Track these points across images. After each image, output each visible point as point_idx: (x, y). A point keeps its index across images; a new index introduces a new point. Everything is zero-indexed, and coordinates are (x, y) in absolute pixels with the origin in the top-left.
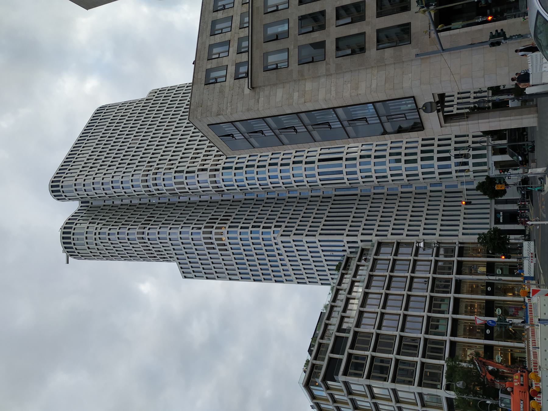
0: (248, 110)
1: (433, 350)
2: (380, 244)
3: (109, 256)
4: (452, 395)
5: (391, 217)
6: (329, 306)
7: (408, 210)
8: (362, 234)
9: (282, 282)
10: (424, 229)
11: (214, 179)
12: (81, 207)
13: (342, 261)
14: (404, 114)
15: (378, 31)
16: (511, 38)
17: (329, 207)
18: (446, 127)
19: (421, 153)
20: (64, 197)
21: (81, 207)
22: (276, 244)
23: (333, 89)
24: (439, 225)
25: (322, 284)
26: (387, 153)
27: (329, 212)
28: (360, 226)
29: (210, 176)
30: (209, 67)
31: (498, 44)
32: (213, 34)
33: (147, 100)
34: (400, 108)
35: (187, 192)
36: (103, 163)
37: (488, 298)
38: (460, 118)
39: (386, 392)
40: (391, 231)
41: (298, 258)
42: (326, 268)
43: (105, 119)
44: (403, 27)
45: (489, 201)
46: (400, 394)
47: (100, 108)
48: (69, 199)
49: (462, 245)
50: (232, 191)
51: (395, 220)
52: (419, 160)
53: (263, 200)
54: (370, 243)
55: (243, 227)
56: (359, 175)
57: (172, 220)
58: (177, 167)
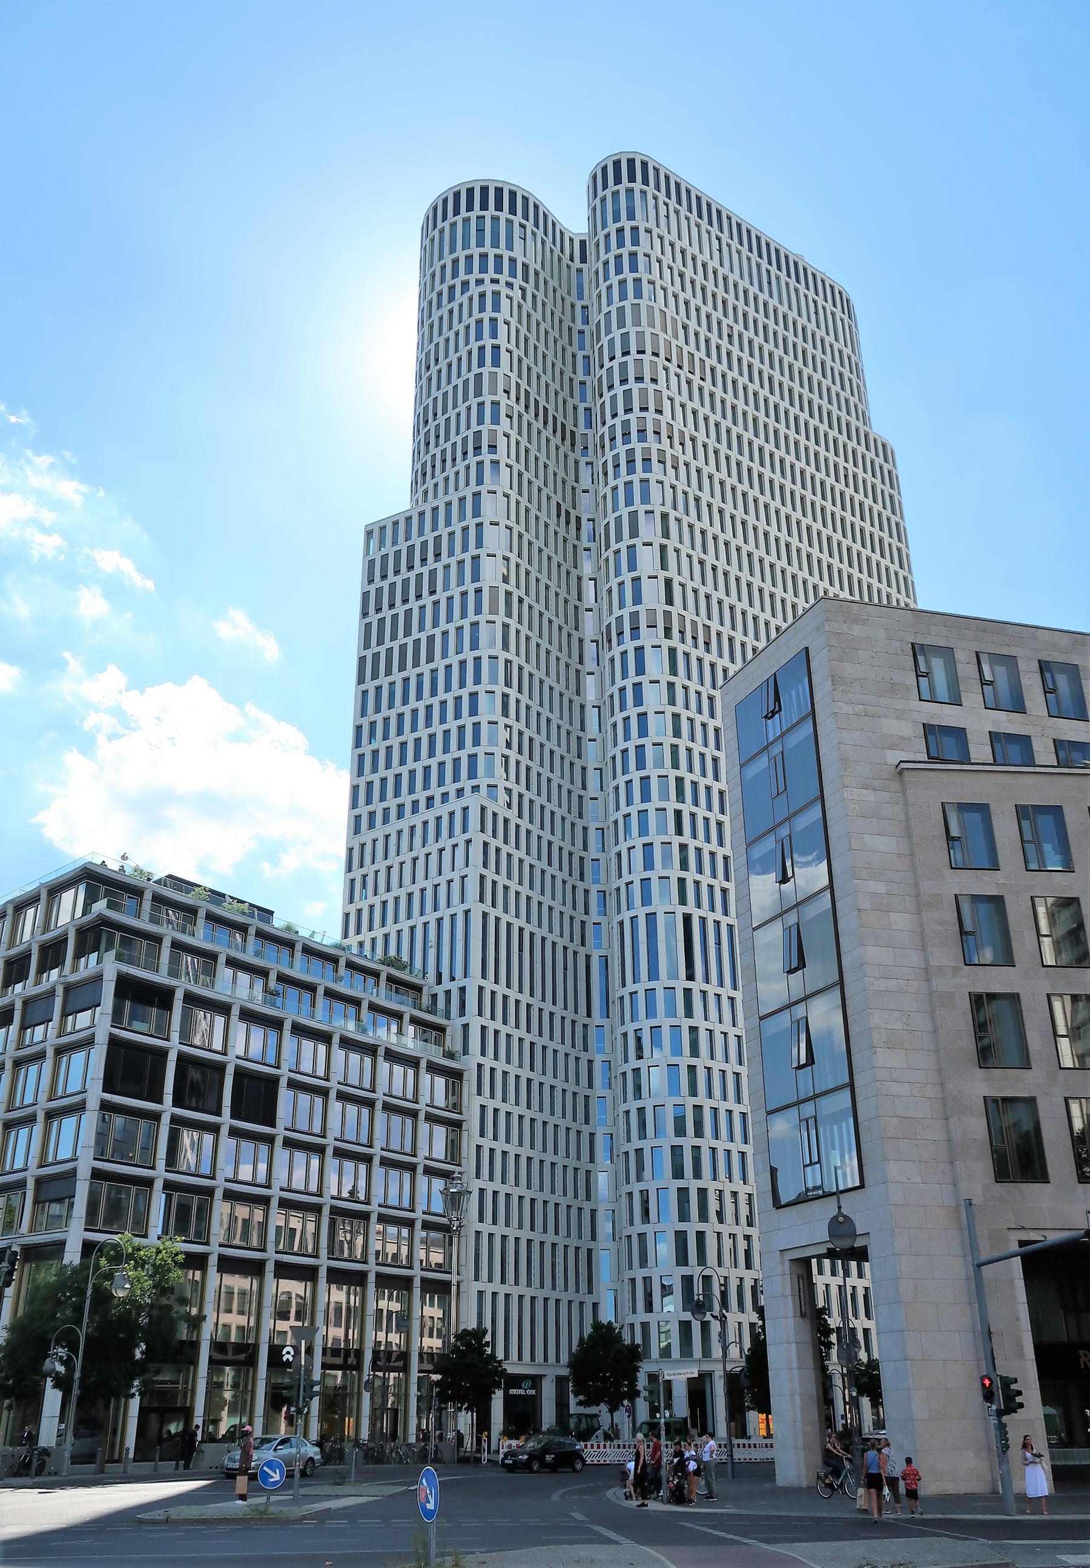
0: (844, 760)
1: (183, 1212)
2: (455, 1076)
3: (430, 317)
4: (72, 1256)
5: (529, 1107)
6: (294, 937)
7: (545, 1150)
8: (484, 1028)
9: (354, 804)
10: (495, 1193)
11: (643, 623)
12: (571, 240)
13: (411, 973)
14: (819, 1162)
15: (1031, 1101)
16: (1002, 1428)
17: (558, 940)
18: (782, 1263)
20: (600, 194)
21: (571, 240)
22: (460, 792)
23: (891, 984)
24: (506, 1231)
25: (347, 916)
27: (543, 939)
28: (505, 1022)
29: (652, 612)
30: (959, 655)
31: (988, 1396)
32: (1044, 667)
33: (866, 436)
34: (833, 1148)
35: (608, 547)
36: (667, 243)
37: (365, 1356)
38: (802, 1297)
39: (74, 1086)
40: (491, 1105)
41: (419, 852)
42: (391, 928)
43: (816, 313)
44: (1033, 1141)
45: (565, 1358)
46: (69, 1123)
47: (847, 301)
48: (594, 209)
49: (454, 1289)
50: (608, 671)
51: (521, 1117)
52: (681, 1183)
53: (579, 757)
54: (458, 1047)
55: (507, 701)
57: (530, 501)
58: (678, 520)
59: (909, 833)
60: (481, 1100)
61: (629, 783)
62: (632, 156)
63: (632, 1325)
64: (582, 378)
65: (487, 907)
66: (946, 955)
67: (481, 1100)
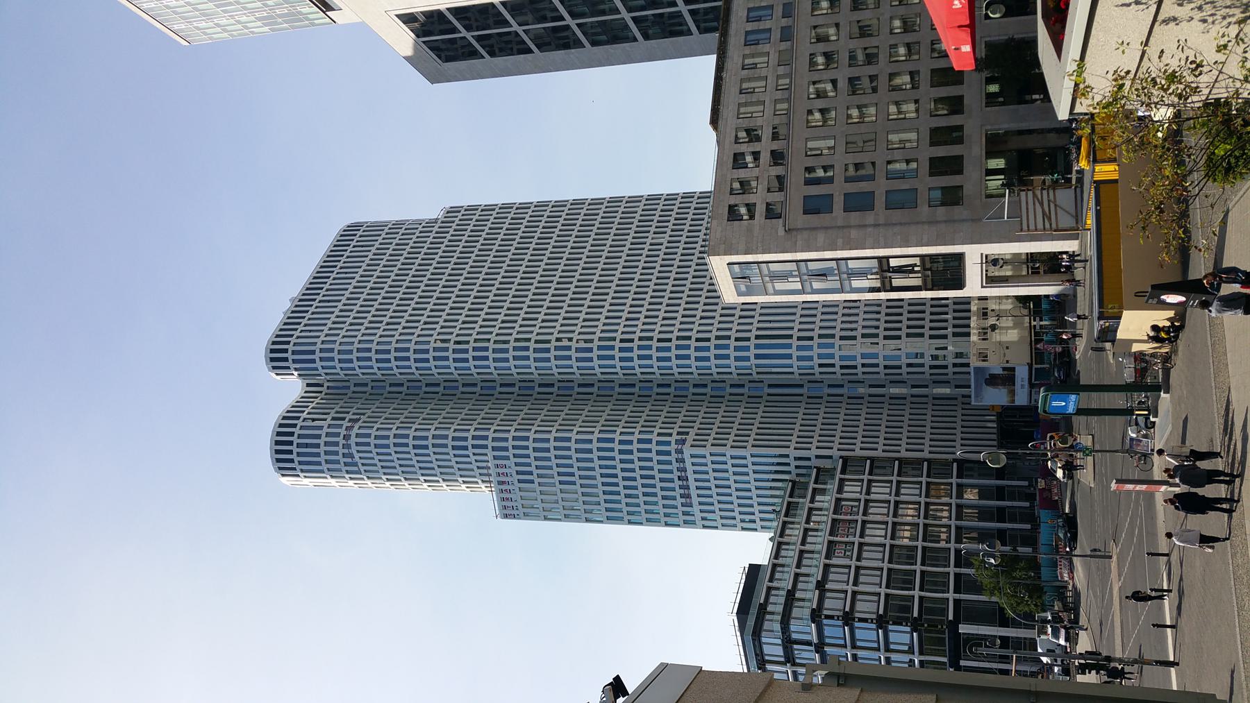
12: (306, 392)
19: (856, 337)
21: (306, 392)
26: (815, 334)
47: (349, 227)
56: (596, 363)
60: (813, 448)
61: (600, 366)
62: (269, 351)
64: (479, 388)
65: (709, 444)
66: (869, 218)
67: (857, 450)
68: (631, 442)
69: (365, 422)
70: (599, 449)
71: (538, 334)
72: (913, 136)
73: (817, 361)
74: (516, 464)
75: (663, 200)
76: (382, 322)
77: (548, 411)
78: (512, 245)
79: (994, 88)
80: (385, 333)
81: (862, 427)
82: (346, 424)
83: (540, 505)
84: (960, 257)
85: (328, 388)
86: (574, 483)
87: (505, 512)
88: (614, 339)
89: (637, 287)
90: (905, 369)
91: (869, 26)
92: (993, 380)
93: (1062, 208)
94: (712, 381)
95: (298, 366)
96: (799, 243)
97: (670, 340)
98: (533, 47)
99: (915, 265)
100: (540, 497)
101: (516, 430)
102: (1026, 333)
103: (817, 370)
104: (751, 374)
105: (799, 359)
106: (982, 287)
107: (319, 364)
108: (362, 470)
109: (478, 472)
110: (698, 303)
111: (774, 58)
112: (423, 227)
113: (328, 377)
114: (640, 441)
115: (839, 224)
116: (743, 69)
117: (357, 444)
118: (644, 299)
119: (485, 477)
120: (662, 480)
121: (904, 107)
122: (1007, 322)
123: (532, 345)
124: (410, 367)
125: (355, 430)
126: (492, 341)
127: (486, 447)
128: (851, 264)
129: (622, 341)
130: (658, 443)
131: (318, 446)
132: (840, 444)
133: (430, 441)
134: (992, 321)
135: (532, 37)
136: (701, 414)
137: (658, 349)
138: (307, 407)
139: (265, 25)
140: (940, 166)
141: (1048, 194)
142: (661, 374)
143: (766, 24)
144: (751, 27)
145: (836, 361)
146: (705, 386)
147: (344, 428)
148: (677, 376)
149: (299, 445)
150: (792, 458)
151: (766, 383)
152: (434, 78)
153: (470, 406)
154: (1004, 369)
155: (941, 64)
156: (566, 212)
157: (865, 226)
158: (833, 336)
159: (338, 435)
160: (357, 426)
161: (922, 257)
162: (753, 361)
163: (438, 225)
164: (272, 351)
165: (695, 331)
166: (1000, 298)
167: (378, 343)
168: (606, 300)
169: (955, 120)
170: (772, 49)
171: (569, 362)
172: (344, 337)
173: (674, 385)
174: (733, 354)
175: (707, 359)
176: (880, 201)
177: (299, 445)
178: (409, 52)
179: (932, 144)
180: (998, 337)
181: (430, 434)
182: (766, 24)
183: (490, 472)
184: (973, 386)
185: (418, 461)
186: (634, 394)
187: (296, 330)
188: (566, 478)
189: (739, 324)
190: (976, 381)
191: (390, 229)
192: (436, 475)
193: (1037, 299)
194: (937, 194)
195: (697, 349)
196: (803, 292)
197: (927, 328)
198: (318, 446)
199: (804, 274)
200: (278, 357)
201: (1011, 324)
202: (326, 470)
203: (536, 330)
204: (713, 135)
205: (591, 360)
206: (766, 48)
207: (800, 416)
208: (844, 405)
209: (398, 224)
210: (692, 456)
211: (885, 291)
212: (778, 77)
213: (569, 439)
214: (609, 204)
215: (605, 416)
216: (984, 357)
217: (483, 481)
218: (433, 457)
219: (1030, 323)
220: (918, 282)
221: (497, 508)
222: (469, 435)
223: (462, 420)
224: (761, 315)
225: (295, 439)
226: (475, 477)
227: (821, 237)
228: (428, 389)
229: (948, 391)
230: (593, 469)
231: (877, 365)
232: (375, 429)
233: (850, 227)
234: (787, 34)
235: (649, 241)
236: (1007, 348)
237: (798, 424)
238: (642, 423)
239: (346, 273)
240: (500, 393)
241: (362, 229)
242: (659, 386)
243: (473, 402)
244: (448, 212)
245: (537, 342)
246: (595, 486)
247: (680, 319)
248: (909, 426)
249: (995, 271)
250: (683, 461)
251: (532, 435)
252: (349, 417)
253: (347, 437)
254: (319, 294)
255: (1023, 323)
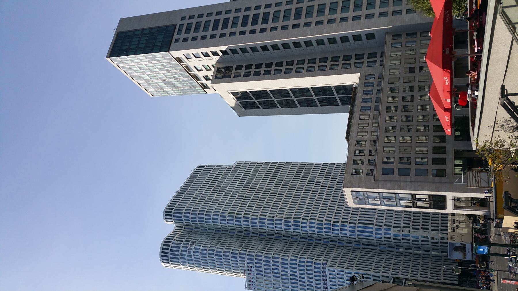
12: (176, 229)
19: (419, 228)
21: (176, 229)
59: (387, 181)
60: (381, 272)
63: (431, 246)
64: (229, 232)
66: (408, 178)
68: (304, 262)
69: (197, 243)
70: (290, 264)
71: (253, 212)
72: (425, 149)
73: (383, 236)
74: (256, 267)
75: (322, 165)
76: (209, 204)
77: (254, 244)
78: (261, 178)
79: (458, 134)
80: (210, 208)
81: (384, 263)
82: (190, 243)
83: (264, 285)
84: (444, 197)
85: (185, 228)
86: (279, 277)
87: (250, 287)
88: (266, 216)
89: (310, 198)
90: (420, 243)
91: (408, 106)
92: (457, 249)
93: (483, 180)
94: (339, 240)
95: (175, 218)
96: (380, 185)
97: (322, 221)
98: (279, 106)
99: (426, 198)
100: (282, 284)
101: (257, 252)
102: (471, 231)
103: (384, 239)
104: (356, 238)
105: (376, 234)
106: (453, 209)
107: (183, 218)
108: (194, 263)
109: (240, 268)
110: (305, 205)
111: (371, 117)
112: (228, 168)
113: (186, 224)
114: (308, 262)
115: (396, 180)
116: (359, 119)
117: (194, 252)
118: (313, 203)
119: (243, 271)
120: (316, 280)
121: (406, 138)
122: (463, 225)
123: (250, 216)
124: (218, 222)
125: (194, 246)
126: (235, 214)
127: (244, 258)
128: (401, 196)
129: (303, 219)
130: (315, 263)
131: (178, 251)
132: (347, 266)
133: (223, 253)
134: (457, 224)
135: (242, 104)
136: (318, 251)
137: (317, 224)
138: (176, 235)
139: (182, 92)
140: (436, 161)
141: (478, 174)
142: (318, 235)
143: (369, 104)
144: (363, 105)
145: (391, 236)
146: (336, 242)
147: (189, 245)
148: (324, 236)
149: (171, 250)
150: (372, 275)
151: (387, 245)
152: (240, 114)
153: (224, 239)
154: (462, 244)
155: (437, 123)
156: (283, 167)
157: (407, 181)
158: (390, 226)
159: (186, 247)
160: (194, 244)
161: (429, 195)
162: (357, 233)
163: (233, 168)
164: (166, 212)
165: (333, 218)
166: (460, 215)
167: (221, 213)
168: (297, 202)
169: (443, 145)
170: (371, 113)
171: (298, 228)
172: (194, 208)
173: (338, 241)
174: (316, 226)
175: (337, 230)
176: (413, 172)
177: (171, 250)
178: (233, 105)
179: (434, 153)
180: (459, 231)
181: (238, 252)
182: (369, 104)
183: (245, 269)
184: (449, 252)
185: (202, 260)
186: (289, 240)
187: (176, 204)
188: (276, 275)
189: (319, 215)
190: (450, 248)
191: (215, 168)
192: (223, 268)
193: (474, 216)
194: (435, 172)
195: (333, 226)
196: (381, 205)
197: (430, 226)
198: (178, 251)
199: (366, 197)
200: (168, 214)
201: (464, 226)
202: (180, 262)
203: (269, 212)
204: (346, 142)
205: (290, 226)
206: (369, 113)
207: (350, 255)
208: (377, 254)
209: (218, 167)
210: (329, 271)
211: (414, 208)
212: (373, 123)
213: (261, 256)
214: (301, 165)
215: (294, 250)
216: (453, 238)
217: (242, 273)
218: (223, 260)
219: (472, 226)
220: (427, 205)
221: (246, 285)
222: (238, 252)
223: (221, 244)
224: (360, 214)
225: (170, 248)
226: (239, 270)
227: (389, 184)
228: (210, 231)
229: (438, 253)
230: (287, 272)
231: (409, 240)
232: (201, 246)
233: (400, 181)
234: (377, 108)
235: (316, 181)
236: (463, 236)
237: (332, 257)
238: (309, 254)
239: (197, 184)
240: (252, 236)
241: (205, 167)
242: (316, 239)
243: (226, 237)
244: (237, 164)
245: (252, 215)
246: (288, 279)
247: (327, 213)
248: (385, 263)
249: (458, 203)
250: (325, 272)
251: (263, 255)
252: (192, 240)
253: (190, 249)
254: (186, 191)
255: (469, 226)
